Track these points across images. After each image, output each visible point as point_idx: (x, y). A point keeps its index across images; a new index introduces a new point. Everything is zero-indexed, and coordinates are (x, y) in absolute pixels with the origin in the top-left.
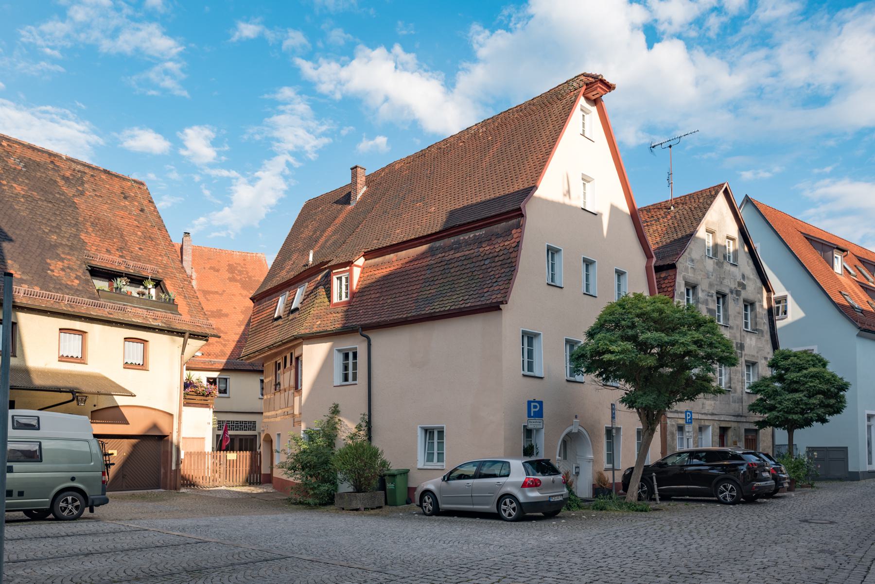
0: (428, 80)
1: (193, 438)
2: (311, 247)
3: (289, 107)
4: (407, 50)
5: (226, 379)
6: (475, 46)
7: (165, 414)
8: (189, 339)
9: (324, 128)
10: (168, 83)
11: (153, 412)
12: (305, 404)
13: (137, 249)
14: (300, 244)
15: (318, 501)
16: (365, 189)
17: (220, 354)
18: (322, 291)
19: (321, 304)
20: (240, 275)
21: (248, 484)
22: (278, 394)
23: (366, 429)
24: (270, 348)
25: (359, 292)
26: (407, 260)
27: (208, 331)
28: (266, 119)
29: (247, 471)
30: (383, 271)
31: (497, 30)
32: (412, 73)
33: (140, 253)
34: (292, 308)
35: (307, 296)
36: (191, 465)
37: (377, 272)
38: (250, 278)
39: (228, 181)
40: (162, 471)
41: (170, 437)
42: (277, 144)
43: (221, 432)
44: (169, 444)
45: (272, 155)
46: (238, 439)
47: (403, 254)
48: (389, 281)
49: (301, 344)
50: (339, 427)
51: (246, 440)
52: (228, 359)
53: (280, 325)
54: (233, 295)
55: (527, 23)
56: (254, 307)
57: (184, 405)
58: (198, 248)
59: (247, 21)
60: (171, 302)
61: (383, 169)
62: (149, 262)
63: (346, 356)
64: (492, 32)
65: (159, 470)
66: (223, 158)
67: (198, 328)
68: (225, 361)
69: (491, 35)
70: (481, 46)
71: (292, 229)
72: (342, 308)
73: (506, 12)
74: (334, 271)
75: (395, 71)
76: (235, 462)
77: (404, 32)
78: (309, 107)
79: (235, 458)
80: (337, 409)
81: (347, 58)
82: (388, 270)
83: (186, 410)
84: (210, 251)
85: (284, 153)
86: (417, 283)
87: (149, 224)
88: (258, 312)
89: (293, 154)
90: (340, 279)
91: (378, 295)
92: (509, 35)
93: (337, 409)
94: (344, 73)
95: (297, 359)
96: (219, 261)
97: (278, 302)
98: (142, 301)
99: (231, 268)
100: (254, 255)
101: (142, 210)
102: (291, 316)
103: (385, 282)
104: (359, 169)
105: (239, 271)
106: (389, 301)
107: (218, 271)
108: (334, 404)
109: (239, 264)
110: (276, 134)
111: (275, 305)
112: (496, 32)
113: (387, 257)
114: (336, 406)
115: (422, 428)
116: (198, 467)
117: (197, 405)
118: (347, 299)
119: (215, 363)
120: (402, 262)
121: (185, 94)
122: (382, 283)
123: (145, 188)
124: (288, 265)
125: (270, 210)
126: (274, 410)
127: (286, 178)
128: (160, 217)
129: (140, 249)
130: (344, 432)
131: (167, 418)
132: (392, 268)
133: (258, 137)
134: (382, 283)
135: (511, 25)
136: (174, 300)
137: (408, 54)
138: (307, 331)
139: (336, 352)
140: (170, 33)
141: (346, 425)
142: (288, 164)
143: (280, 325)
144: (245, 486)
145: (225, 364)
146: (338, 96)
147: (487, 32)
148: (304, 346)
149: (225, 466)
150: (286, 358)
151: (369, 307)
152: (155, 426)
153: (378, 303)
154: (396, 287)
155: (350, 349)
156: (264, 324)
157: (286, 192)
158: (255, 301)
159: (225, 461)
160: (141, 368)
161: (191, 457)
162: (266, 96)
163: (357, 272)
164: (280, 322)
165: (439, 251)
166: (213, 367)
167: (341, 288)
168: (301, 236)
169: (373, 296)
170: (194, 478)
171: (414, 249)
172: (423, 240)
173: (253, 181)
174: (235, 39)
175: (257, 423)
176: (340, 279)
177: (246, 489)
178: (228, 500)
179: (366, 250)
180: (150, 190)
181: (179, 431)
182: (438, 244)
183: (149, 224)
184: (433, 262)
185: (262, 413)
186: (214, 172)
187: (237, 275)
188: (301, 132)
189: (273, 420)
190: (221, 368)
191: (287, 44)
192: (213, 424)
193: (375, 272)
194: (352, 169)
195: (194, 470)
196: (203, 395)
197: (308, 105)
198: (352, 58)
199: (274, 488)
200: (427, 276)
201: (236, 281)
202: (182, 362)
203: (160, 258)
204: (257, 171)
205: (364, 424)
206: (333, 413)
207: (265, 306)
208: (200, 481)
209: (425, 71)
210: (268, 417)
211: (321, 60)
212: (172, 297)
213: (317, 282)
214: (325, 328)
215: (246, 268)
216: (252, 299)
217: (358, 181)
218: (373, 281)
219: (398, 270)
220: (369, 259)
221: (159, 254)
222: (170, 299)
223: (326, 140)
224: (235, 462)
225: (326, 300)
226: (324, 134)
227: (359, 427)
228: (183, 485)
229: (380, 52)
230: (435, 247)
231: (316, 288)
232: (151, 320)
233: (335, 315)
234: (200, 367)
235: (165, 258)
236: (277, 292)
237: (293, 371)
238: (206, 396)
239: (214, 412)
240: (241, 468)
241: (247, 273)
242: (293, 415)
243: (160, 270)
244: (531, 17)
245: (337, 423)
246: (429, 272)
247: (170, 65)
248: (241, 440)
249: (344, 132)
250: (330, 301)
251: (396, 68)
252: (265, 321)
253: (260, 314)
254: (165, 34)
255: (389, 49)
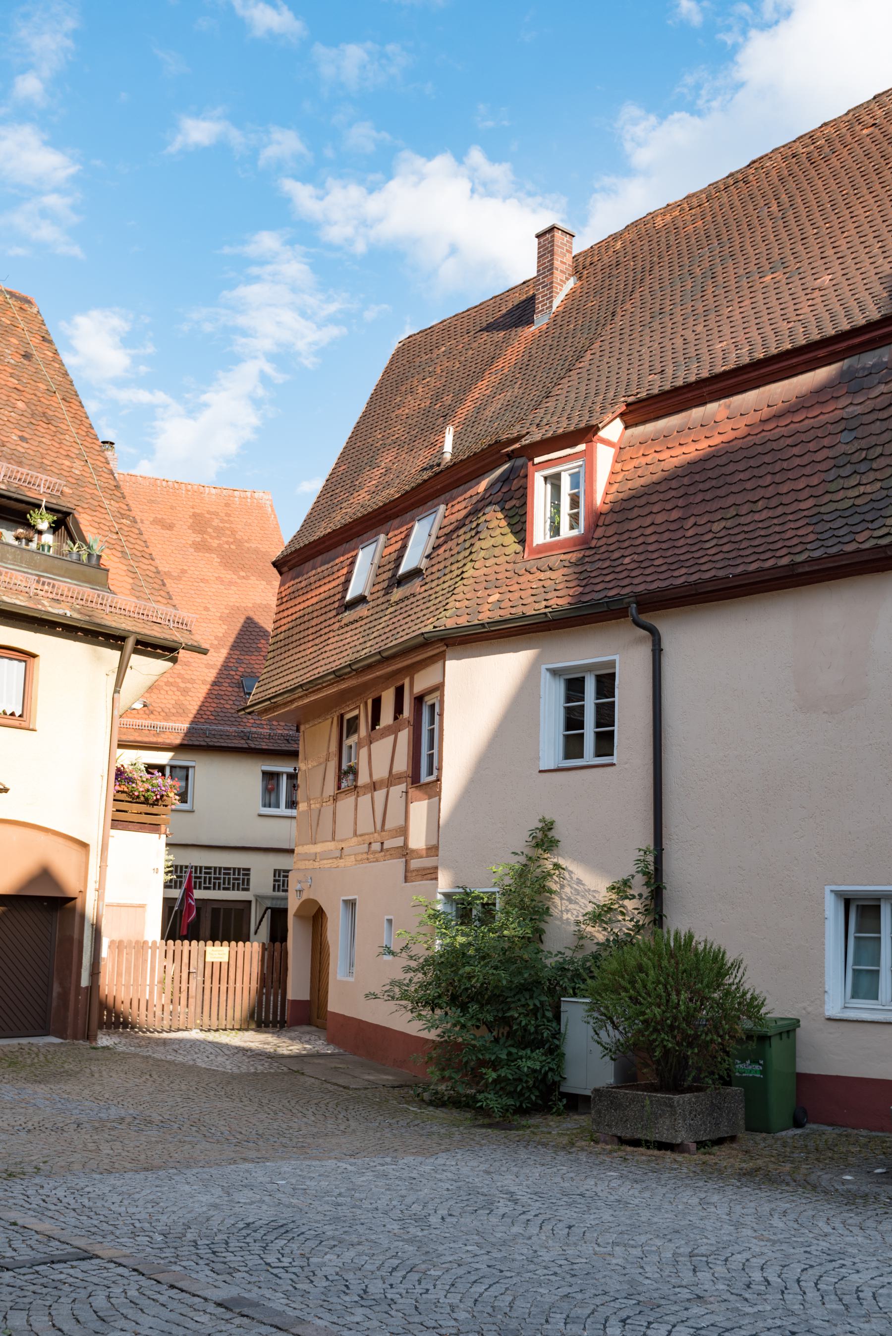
0: (534, 211)
1: (119, 906)
2: (446, 416)
3: (269, 268)
4: (494, 157)
5: (187, 768)
6: (628, 146)
7: (61, 840)
8: (133, 656)
9: (332, 308)
10: (46, 232)
11: (41, 837)
12: (448, 823)
13: (15, 438)
14: (399, 430)
15: (511, 1102)
16: (571, 283)
17: (174, 711)
18: (495, 518)
19: (497, 552)
20: (218, 538)
21: (253, 1026)
22: (347, 803)
23: (646, 892)
24: (338, 675)
25: (611, 511)
26: (766, 412)
27: (178, 637)
28: (225, 293)
29: (253, 992)
30: (684, 449)
31: (672, 114)
32: (505, 199)
33: (22, 447)
34: (348, 598)
35: (446, 536)
36: (119, 975)
37: (665, 455)
38: (239, 543)
39: (149, 413)
40: (56, 989)
41: (79, 902)
42: (243, 340)
43: (177, 893)
44: (77, 919)
45: (236, 360)
46: (209, 910)
47: (751, 398)
48: (710, 474)
49: (441, 657)
50: (555, 887)
51: (228, 911)
52: (192, 722)
53: (361, 618)
54: (203, 580)
55: (732, 99)
56: (282, 584)
57: (113, 827)
58: (128, 479)
59: (197, 115)
60: (94, 561)
61: (615, 237)
62: (42, 468)
63: (574, 687)
64: (663, 117)
65: (49, 987)
66: (143, 369)
67: (155, 627)
68: (185, 726)
69: (660, 124)
70: (640, 145)
71: (369, 404)
72: (563, 557)
73: (689, 80)
74: (537, 460)
75: (471, 197)
76: (224, 967)
77: (490, 124)
78: (306, 267)
79: (225, 959)
80: (550, 834)
81: (378, 177)
82: (704, 444)
83: (120, 837)
84: (155, 485)
85: (256, 358)
86: (807, 470)
87: (42, 387)
88: (293, 596)
89: (272, 358)
90: (554, 481)
91: (675, 515)
92: (696, 121)
93: (550, 834)
94: (374, 205)
95: (419, 700)
96: (172, 508)
97: (353, 563)
98: (27, 555)
99: (199, 523)
100: (249, 494)
101: (27, 356)
102: (397, 594)
103: (697, 478)
104: (558, 234)
105: (216, 529)
106: (716, 527)
107: (170, 527)
108: (543, 820)
109: (216, 514)
110: (242, 321)
111: (345, 571)
112: (671, 117)
113: (697, 413)
114: (548, 827)
115: (837, 894)
116: (136, 980)
117: (131, 826)
118: (575, 533)
119: (163, 730)
120: (748, 420)
121: (76, 251)
122: (686, 481)
123: (35, 310)
124: (372, 479)
125: (224, 465)
126: (334, 839)
127: (257, 403)
128: (66, 374)
129: (22, 438)
130: (570, 900)
131: (75, 852)
132: (716, 440)
133: (208, 327)
134: (686, 481)
135: (700, 103)
136: (99, 557)
137: (497, 165)
138: (463, 621)
139: (546, 677)
140: (55, 143)
141: (579, 882)
142: (264, 379)
143: (361, 618)
144: (247, 1030)
145: (186, 735)
146: (360, 247)
147: (653, 119)
148: (449, 663)
149: (200, 978)
150: (377, 704)
151: (651, 548)
152: (45, 875)
153: (679, 534)
154: (734, 489)
155: (589, 668)
156: (314, 622)
157: (257, 430)
158: (285, 569)
159: (201, 966)
160: (16, 723)
161: (120, 953)
162: (227, 250)
163: (604, 457)
164: (362, 610)
165: (875, 379)
166: (160, 740)
167: (556, 507)
168: (397, 412)
169: (659, 519)
170: (118, 1002)
171: (786, 382)
172: (821, 353)
173: (193, 411)
174: (173, 149)
175: (252, 873)
176: (554, 481)
177: (254, 1040)
178: (231, 1078)
179: (631, 399)
180: (45, 316)
181: (100, 889)
182: (869, 359)
183: (42, 387)
184: (858, 410)
185: (291, 851)
186: (126, 395)
187: (212, 537)
188: (289, 317)
189: (326, 863)
190: (177, 741)
191: (270, 152)
192: (167, 873)
193: (662, 456)
194: (538, 236)
195: (127, 987)
196: (146, 802)
197: (305, 264)
198: (390, 176)
199: (330, 1041)
200: (842, 448)
201: (209, 549)
202: (116, 713)
203: (67, 463)
204: (204, 392)
205: (639, 881)
206: (537, 845)
207: (312, 579)
208: (141, 1017)
209: (530, 194)
210: (306, 857)
211: (330, 182)
212: (97, 549)
213: (475, 499)
214: (518, 611)
215: (231, 522)
216: (278, 565)
217: (557, 263)
218: (655, 478)
219: (739, 444)
220: (636, 425)
221: (65, 453)
222: (90, 555)
223: (334, 331)
224: (224, 967)
225: (510, 538)
226: (332, 320)
227: (621, 888)
228: (101, 1025)
229: (442, 163)
230: (863, 368)
231: (476, 511)
232: (45, 603)
233: (542, 576)
234: (131, 738)
235: (78, 464)
236: (347, 540)
237: (404, 736)
238: (153, 805)
239: (168, 845)
240: (239, 985)
241: (233, 532)
242: (405, 852)
243: (67, 490)
244: (740, 86)
245: (549, 875)
246: (846, 437)
247: (52, 200)
248: (215, 912)
249: (370, 315)
250: (522, 542)
251: (473, 191)
252: (315, 614)
253: (299, 600)
254: (46, 143)
255: (460, 157)
